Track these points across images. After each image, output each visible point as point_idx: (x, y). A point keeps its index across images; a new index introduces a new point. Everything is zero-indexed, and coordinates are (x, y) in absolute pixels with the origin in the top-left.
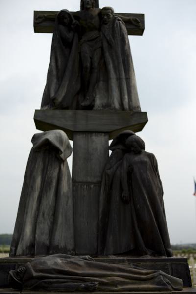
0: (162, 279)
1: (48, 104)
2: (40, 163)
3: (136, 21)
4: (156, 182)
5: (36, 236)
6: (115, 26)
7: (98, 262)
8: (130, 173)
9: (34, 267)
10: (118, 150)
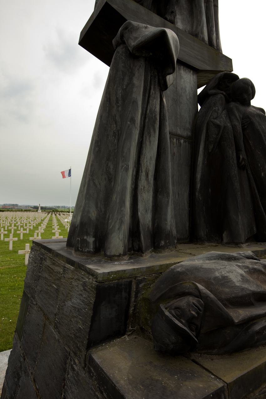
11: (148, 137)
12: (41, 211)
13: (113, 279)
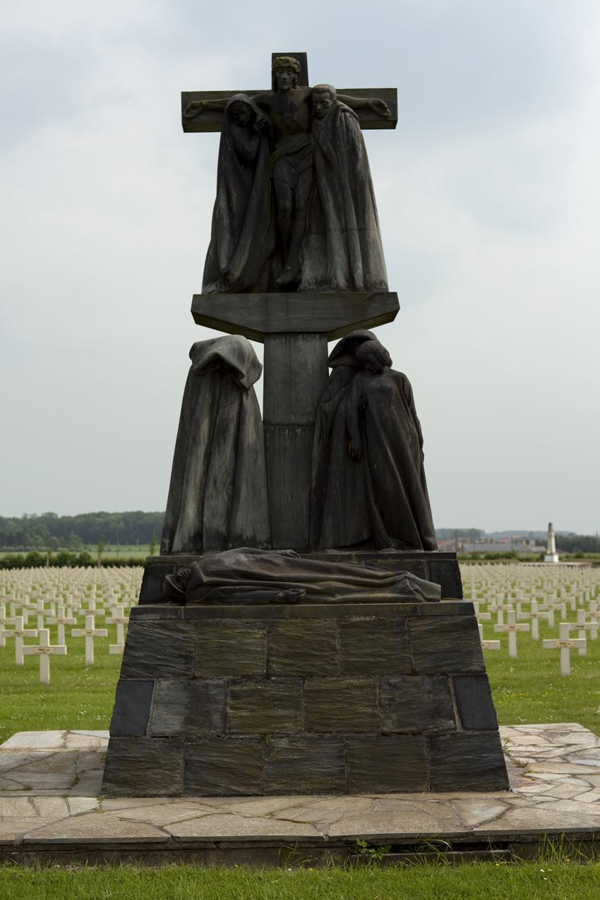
0: (408, 584)
1: (215, 280)
2: (207, 396)
3: (380, 105)
4: (407, 426)
5: (205, 519)
6: (338, 122)
7: (305, 560)
8: (363, 409)
9: (204, 568)
10: (342, 367)
11: (217, 448)
12: (560, 559)
13: (157, 562)
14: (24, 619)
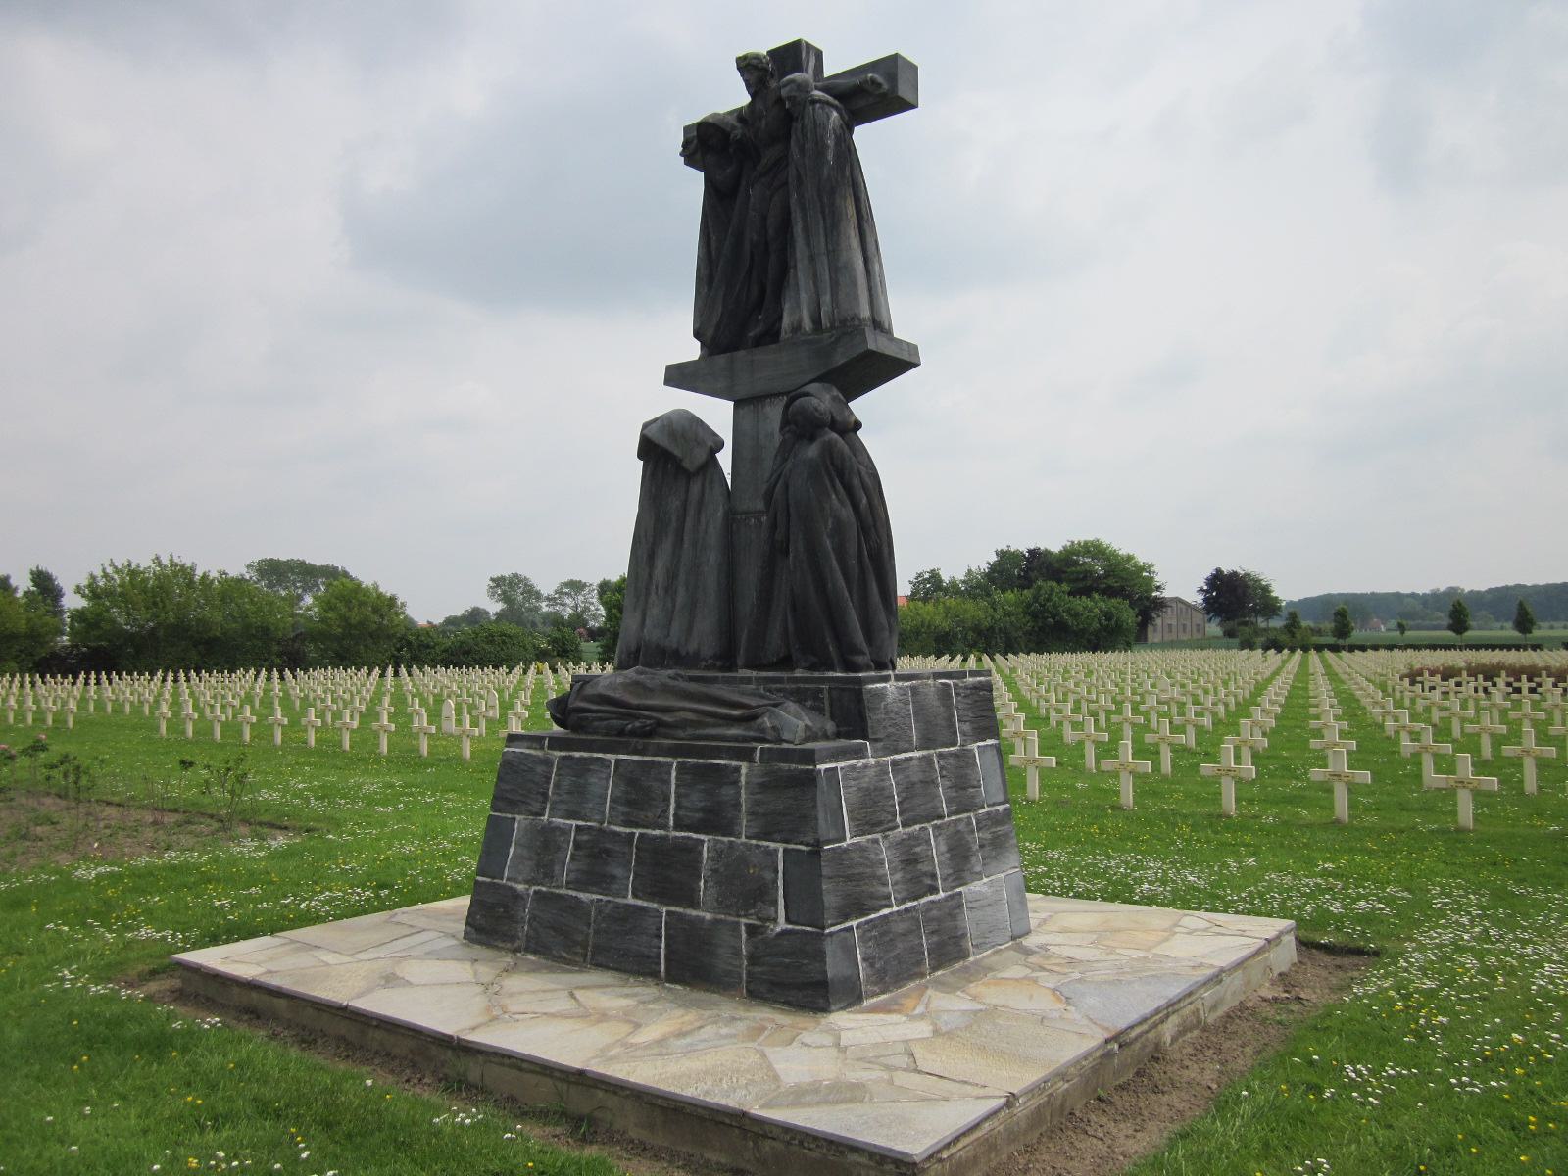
14: (1070, 705)
